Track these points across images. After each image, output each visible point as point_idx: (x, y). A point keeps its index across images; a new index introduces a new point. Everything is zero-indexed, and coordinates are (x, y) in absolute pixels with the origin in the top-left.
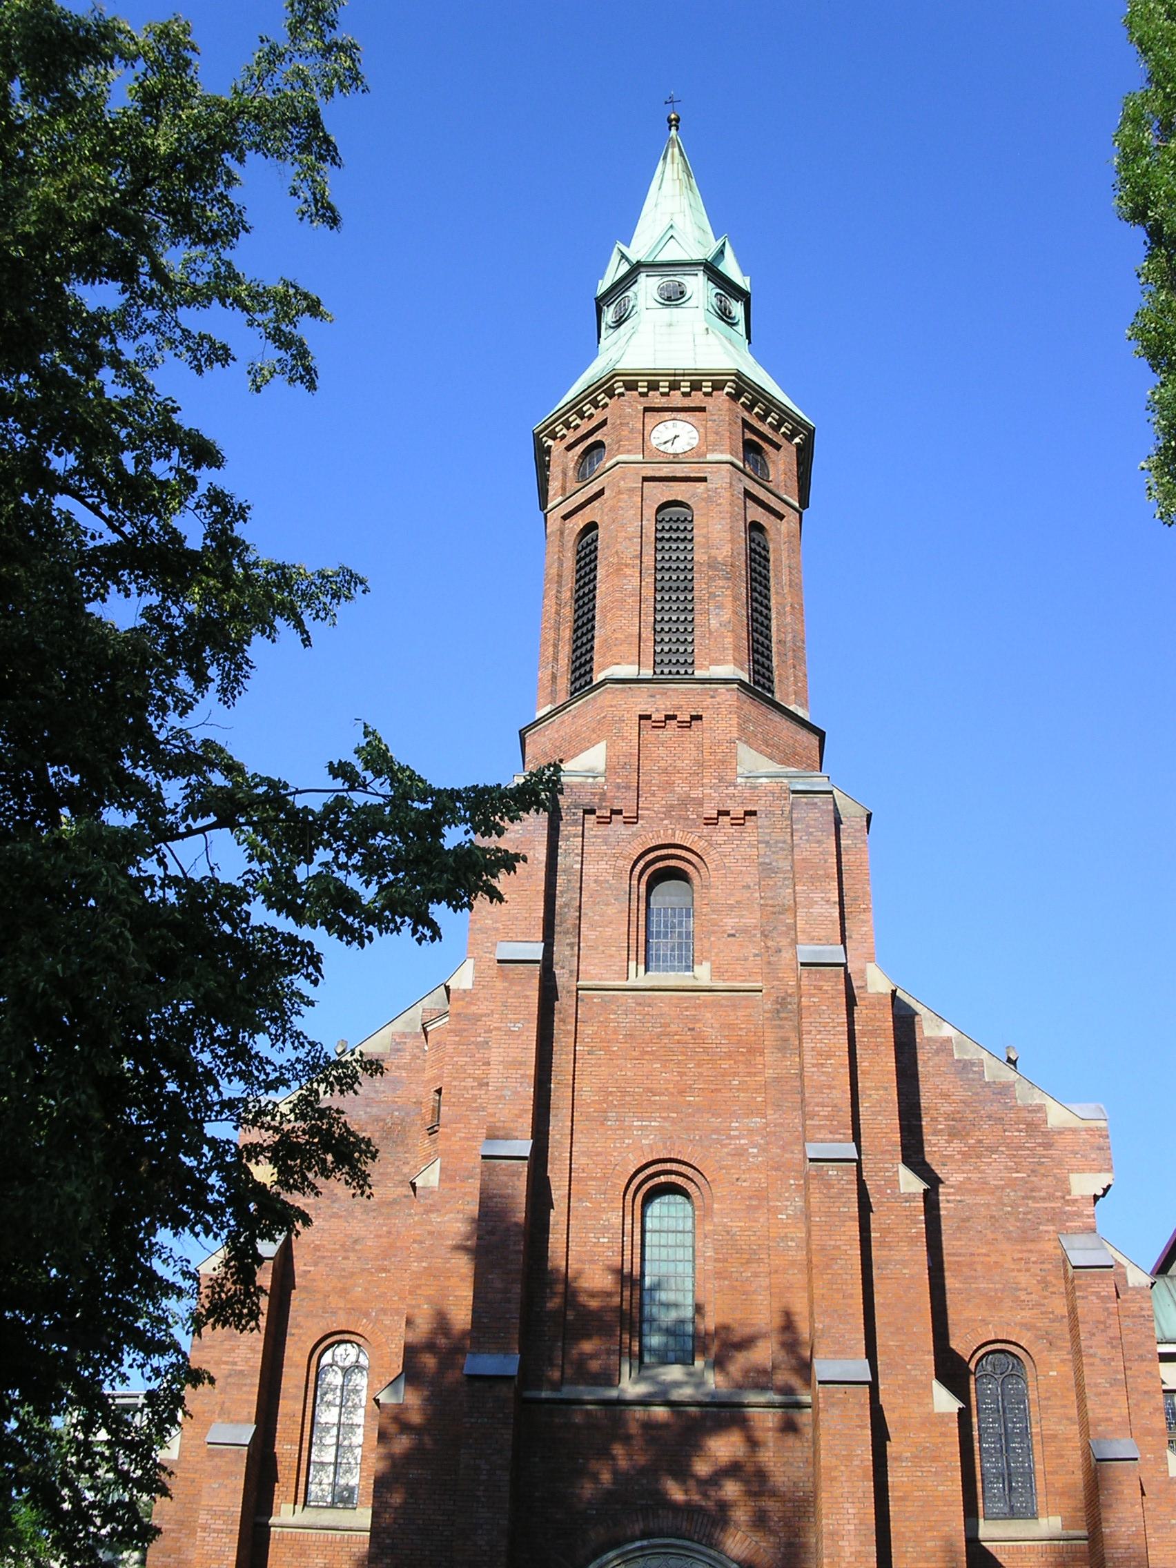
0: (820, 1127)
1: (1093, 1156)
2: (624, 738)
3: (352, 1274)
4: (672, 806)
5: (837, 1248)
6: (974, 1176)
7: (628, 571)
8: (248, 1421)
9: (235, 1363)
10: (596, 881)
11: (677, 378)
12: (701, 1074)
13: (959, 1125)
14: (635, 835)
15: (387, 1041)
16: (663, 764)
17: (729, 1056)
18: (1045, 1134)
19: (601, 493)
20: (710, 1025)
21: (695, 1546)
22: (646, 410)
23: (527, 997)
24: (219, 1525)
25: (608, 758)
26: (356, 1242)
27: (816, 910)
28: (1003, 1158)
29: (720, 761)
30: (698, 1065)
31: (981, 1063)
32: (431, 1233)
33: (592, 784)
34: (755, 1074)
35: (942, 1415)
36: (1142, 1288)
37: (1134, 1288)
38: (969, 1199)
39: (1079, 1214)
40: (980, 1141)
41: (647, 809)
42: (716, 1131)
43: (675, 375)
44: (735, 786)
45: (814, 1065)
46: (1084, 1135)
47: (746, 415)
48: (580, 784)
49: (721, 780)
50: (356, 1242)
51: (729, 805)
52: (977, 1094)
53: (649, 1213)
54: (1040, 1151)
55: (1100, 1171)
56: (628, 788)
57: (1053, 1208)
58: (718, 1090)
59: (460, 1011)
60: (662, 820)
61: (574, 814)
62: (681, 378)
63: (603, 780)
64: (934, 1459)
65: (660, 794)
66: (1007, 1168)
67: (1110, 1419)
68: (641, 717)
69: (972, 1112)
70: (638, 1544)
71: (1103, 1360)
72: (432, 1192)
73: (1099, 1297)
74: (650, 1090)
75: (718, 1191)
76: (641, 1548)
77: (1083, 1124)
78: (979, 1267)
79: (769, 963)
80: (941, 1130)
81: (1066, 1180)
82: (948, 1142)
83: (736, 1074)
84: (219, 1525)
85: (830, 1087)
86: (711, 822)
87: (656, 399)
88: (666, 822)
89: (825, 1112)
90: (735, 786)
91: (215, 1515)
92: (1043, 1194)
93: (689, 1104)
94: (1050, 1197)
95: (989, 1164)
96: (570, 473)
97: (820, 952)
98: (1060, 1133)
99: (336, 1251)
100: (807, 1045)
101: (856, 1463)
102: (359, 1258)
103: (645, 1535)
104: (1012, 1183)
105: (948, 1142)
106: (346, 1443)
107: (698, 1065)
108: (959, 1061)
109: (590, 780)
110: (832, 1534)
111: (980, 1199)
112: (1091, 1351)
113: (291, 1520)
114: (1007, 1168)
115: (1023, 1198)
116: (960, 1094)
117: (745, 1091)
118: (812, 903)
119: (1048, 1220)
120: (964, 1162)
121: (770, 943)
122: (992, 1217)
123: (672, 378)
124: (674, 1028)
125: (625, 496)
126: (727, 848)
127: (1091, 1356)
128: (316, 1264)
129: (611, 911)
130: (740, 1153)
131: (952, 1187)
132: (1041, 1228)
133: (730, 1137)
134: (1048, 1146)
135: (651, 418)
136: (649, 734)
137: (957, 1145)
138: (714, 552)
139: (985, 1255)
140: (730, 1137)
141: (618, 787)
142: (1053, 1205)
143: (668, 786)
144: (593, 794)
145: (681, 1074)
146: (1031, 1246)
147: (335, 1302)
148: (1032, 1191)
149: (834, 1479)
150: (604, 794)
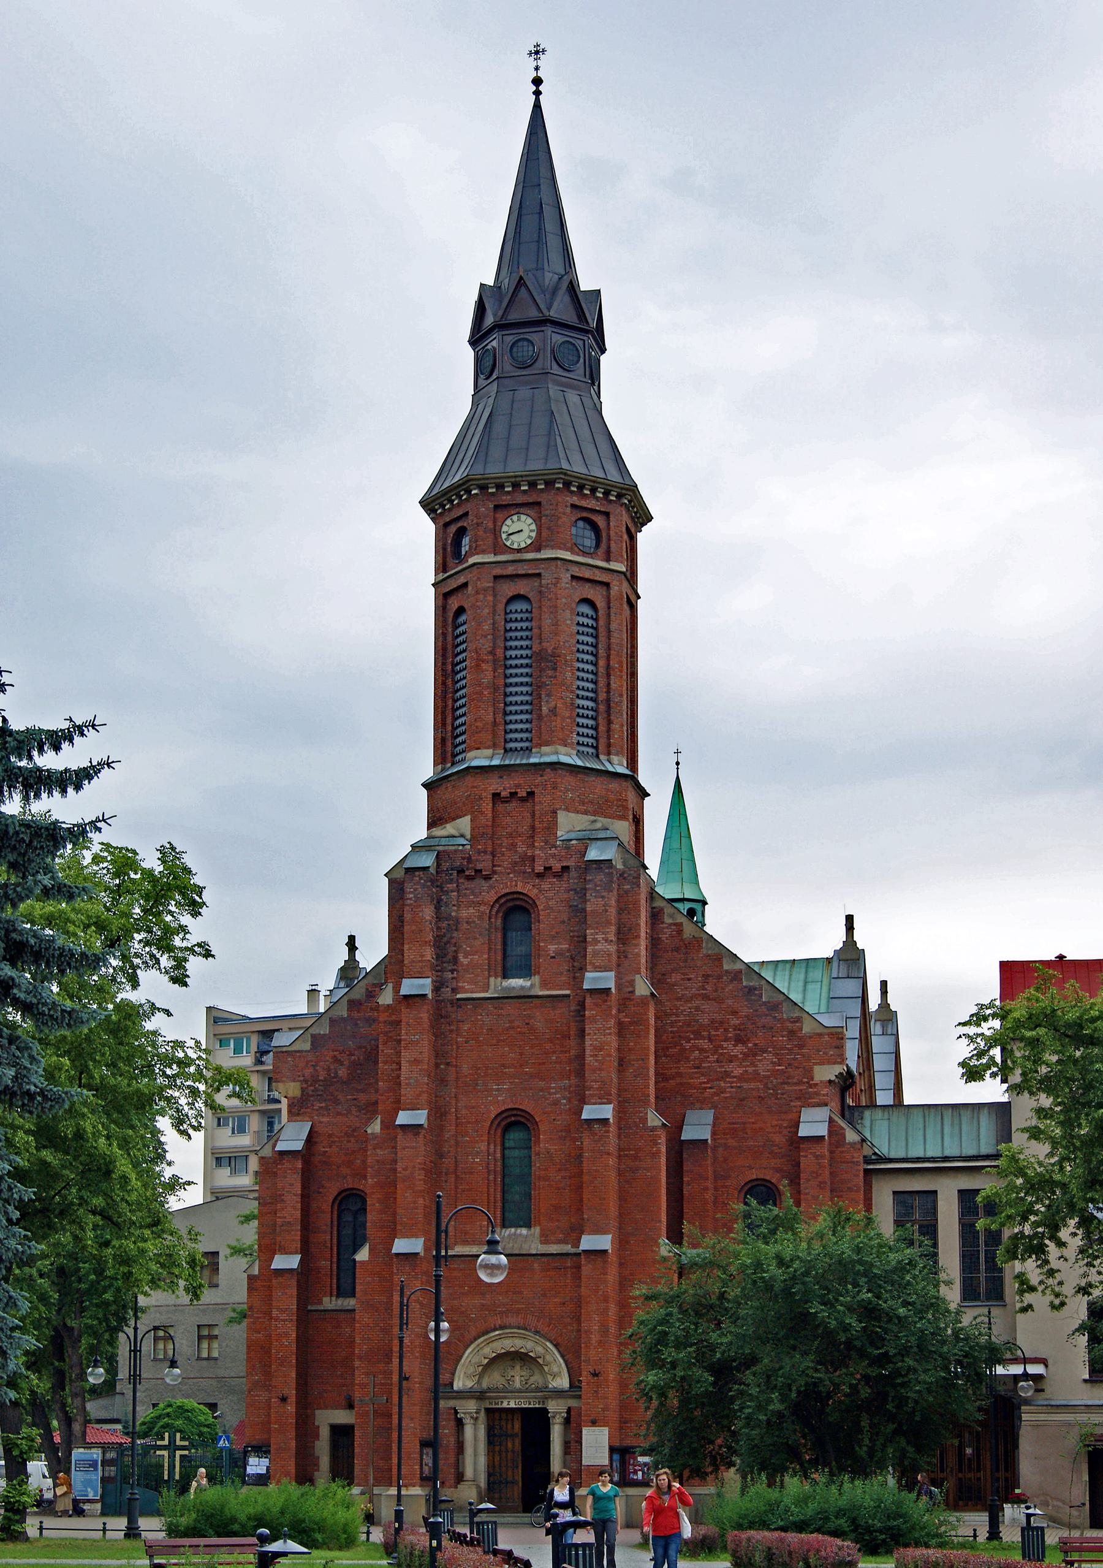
1: (832, 1053)
2: (482, 813)
3: (354, 1152)
4: (516, 863)
6: (750, 1070)
7: (484, 666)
8: (296, 1253)
9: (285, 1218)
10: (467, 923)
11: (518, 479)
12: (533, 1053)
14: (491, 887)
15: (364, 990)
16: (509, 830)
17: (551, 1041)
18: (800, 1038)
19: (465, 585)
20: (539, 1022)
21: (527, 1333)
22: (496, 507)
23: (421, 1018)
24: (284, 1316)
25: (472, 829)
26: (354, 1130)
27: (599, 947)
28: (770, 1056)
29: (546, 828)
30: (532, 1047)
32: (378, 1161)
33: (461, 851)
34: (566, 1052)
36: (855, 1143)
37: (850, 1144)
38: (745, 1085)
39: (817, 1094)
40: (756, 1045)
41: (499, 866)
42: (542, 1090)
43: (516, 477)
44: (556, 847)
45: (591, 1056)
46: (826, 1038)
47: (575, 500)
48: (455, 851)
49: (546, 842)
50: (354, 1130)
52: (757, 1011)
53: (507, 1137)
54: (796, 1050)
55: (834, 1063)
56: (485, 852)
57: (801, 1090)
58: (544, 1063)
59: (386, 1019)
60: (509, 874)
61: (451, 874)
62: (520, 479)
63: (469, 847)
65: (508, 853)
66: (772, 1063)
68: (494, 794)
69: (752, 1024)
70: (497, 1333)
71: (813, 1196)
72: (377, 1137)
74: (503, 1065)
75: (542, 1128)
76: (499, 1335)
77: (826, 1031)
78: (749, 1131)
79: (574, 978)
80: (731, 1038)
81: (811, 1070)
82: (735, 1046)
83: (554, 1052)
84: (284, 1316)
85: (600, 1070)
87: (505, 499)
88: (511, 875)
90: (556, 847)
91: (282, 1311)
92: (795, 1081)
93: (526, 1073)
94: (800, 1083)
95: (760, 1061)
97: (599, 978)
98: (810, 1037)
99: (342, 1137)
100: (588, 1042)
101: (600, 1293)
102: (357, 1141)
103: (502, 1328)
104: (775, 1073)
105: (735, 1046)
107: (532, 1047)
108: (746, 987)
109: (461, 848)
111: (752, 1085)
112: (807, 1191)
113: (330, 1306)
114: (772, 1063)
115: (782, 1083)
116: (745, 1011)
117: (560, 1063)
118: (596, 942)
119: (796, 1099)
120: (744, 1060)
121: (576, 964)
122: (759, 1097)
123: (513, 480)
124: (516, 1023)
125: (481, 596)
127: (806, 1194)
128: (330, 1147)
129: (477, 943)
130: (556, 1103)
131: (735, 1077)
132: (792, 1104)
133: (550, 1094)
134: (801, 1047)
135: (500, 515)
136: (501, 807)
137: (740, 1047)
139: (753, 1123)
140: (550, 1094)
141: (479, 852)
142: (801, 1088)
143: (513, 846)
144: (463, 858)
145: (521, 1054)
146: (784, 1116)
147: (345, 1170)
148: (788, 1078)
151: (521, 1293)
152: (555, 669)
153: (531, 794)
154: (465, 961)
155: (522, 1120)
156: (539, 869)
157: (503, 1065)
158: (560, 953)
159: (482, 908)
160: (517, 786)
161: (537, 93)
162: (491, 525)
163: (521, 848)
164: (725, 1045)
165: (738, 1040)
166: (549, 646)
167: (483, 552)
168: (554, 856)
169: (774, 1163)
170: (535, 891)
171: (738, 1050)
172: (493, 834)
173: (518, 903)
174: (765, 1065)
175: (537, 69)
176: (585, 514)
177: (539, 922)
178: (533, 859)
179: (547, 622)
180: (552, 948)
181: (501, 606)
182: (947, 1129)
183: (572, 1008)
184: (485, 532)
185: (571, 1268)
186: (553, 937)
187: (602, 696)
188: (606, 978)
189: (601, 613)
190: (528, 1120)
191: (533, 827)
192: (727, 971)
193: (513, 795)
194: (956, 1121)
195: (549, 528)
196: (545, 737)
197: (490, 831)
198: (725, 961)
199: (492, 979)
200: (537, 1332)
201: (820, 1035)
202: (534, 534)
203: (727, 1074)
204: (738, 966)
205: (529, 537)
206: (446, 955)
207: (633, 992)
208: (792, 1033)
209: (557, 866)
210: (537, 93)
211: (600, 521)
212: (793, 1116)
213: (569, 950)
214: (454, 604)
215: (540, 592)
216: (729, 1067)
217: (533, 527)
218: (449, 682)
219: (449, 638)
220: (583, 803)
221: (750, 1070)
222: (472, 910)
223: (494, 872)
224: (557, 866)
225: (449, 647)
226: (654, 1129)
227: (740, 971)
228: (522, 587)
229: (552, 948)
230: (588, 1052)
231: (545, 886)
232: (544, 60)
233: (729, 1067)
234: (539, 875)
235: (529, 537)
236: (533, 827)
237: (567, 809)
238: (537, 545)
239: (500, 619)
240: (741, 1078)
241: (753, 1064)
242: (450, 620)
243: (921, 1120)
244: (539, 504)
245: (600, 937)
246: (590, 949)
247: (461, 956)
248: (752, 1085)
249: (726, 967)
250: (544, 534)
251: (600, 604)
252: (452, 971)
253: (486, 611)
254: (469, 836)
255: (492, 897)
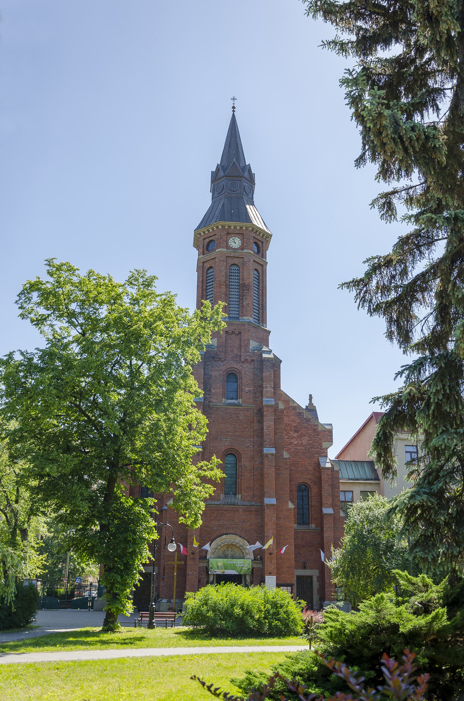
0: (267, 444)
5: (270, 473)
6: (300, 442)
7: (222, 286)
13: (297, 429)
14: (224, 365)
16: (231, 345)
18: (317, 432)
28: (307, 438)
31: (303, 413)
35: (290, 509)
38: (298, 448)
40: (302, 433)
48: (211, 350)
51: (248, 358)
56: (222, 352)
64: (288, 518)
67: (327, 503)
73: (327, 474)
74: (228, 432)
81: (321, 444)
86: (243, 362)
89: (268, 440)
90: (249, 352)
93: (237, 435)
96: (205, 247)
103: (226, 534)
106: (165, 508)
110: (267, 537)
111: (300, 448)
118: (267, 387)
124: (233, 416)
125: (221, 262)
126: (246, 369)
130: (248, 447)
133: (246, 443)
134: (318, 435)
135: (228, 237)
137: (296, 434)
138: (245, 282)
141: (220, 352)
143: (232, 351)
145: (235, 427)
146: (312, 460)
149: (267, 525)
150: (217, 353)
151: (234, 520)
152: (249, 290)
153: (240, 333)
154: (214, 391)
155: (234, 453)
156: (243, 359)
157: (228, 432)
158: (250, 391)
159: (221, 372)
160: (235, 329)
161: (234, 111)
162: (225, 239)
163: (236, 352)
164: (291, 432)
165: (296, 431)
166: (246, 282)
167: (223, 248)
168: (248, 356)
169: (309, 477)
170: (241, 368)
171: (295, 435)
172: (226, 345)
173: (233, 372)
174: (305, 441)
175: (234, 104)
176: (256, 241)
177: (242, 379)
178: (240, 356)
179: (246, 274)
180: (247, 389)
181: (228, 267)
182: (360, 469)
183: (255, 412)
184: (223, 241)
185: (255, 511)
186: (247, 385)
187: (261, 303)
188: (271, 401)
189: (260, 275)
190: (236, 453)
191: (240, 345)
192: (291, 406)
193: (233, 332)
194: (357, 467)
195: (247, 243)
196: (244, 314)
197: (224, 344)
198: (290, 402)
199: (223, 399)
200: (240, 537)
201: (325, 431)
202: (240, 244)
203: (292, 443)
204: (295, 405)
205: (239, 245)
206: (207, 388)
207: (278, 407)
208: (315, 430)
209: (249, 359)
210: (234, 111)
211: (260, 243)
212: (315, 460)
213: (253, 390)
214: (207, 265)
215: (243, 264)
216: (292, 441)
217: (240, 242)
218: (204, 292)
219: (205, 277)
220: (257, 338)
221: (300, 442)
222: (216, 373)
223: (225, 360)
224: (249, 359)
225: (205, 280)
226: (286, 459)
227: (296, 407)
228: (236, 261)
229: (247, 389)
230: (265, 428)
231: (244, 366)
232: (236, 102)
233: (292, 441)
234: (243, 362)
235: (239, 245)
236: (240, 345)
237: (252, 339)
238: (242, 248)
239: (228, 271)
240: (296, 445)
241: (301, 440)
242: (205, 271)
243: (344, 465)
244: (243, 234)
245: (268, 386)
246: (265, 390)
247: (212, 389)
248: (300, 448)
249: (291, 405)
250: (245, 244)
251: (260, 272)
252: (209, 395)
253: (223, 268)
254: (216, 345)
255: (224, 368)
